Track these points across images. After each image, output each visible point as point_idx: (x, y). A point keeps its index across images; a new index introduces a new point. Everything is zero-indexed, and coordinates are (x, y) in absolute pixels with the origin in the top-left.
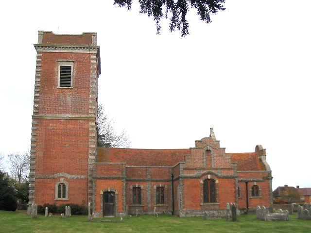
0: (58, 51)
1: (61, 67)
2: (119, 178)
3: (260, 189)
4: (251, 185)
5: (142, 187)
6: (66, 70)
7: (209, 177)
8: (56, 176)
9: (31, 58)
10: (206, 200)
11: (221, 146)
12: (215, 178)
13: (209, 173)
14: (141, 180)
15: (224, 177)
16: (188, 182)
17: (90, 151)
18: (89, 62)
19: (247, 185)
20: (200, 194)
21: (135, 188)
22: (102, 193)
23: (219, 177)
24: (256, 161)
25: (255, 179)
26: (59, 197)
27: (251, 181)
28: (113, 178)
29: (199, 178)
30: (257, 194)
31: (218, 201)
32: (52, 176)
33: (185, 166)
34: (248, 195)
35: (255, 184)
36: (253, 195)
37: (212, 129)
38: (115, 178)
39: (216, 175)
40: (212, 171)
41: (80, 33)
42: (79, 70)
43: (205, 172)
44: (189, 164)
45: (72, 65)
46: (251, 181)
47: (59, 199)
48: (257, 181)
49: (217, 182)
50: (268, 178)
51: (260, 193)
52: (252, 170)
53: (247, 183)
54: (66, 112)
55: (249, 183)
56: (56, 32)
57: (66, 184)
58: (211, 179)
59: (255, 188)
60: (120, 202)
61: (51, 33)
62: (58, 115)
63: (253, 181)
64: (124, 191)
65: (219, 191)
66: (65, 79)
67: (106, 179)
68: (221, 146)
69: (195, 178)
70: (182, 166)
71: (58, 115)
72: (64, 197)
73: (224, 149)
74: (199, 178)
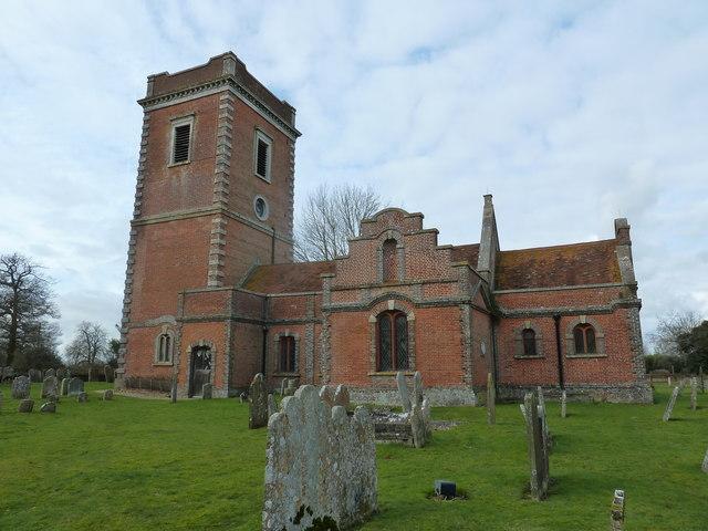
0: (171, 103)
1: (177, 129)
2: (219, 320)
3: (599, 334)
4: (570, 324)
7: (391, 305)
8: (156, 321)
9: (134, 121)
10: (382, 365)
11: (427, 225)
14: (295, 323)
15: (429, 305)
16: (341, 321)
17: (210, 273)
19: (557, 325)
20: (370, 346)
21: (283, 339)
22: (189, 350)
24: (602, 266)
26: (161, 359)
27: (572, 314)
29: (366, 309)
30: (592, 347)
31: (412, 365)
32: (151, 322)
33: (334, 283)
34: (563, 350)
35: (583, 319)
36: (579, 349)
37: (488, 198)
39: (409, 301)
40: (397, 290)
41: (206, 61)
43: (380, 293)
44: (344, 278)
45: (189, 122)
46: (572, 314)
47: (160, 363)
48: (588, 313)
49: (411, 316)
50: (630, 301)
51: (600, 345)
52: (586, 283)
54: (178, 206)
55: (565, 319)
56: (171, 72)
58: (395, 311)
60: (219, 372)
61: (164, 75)
62: (167, 214)
63: (577, 313)
64: (228, 345)
66: (181, 152)
68: (427, 225)
69: (357, 309)
70: (326, 284)
72: (167, 360)
73: (436, 232)
74: (366, 309)
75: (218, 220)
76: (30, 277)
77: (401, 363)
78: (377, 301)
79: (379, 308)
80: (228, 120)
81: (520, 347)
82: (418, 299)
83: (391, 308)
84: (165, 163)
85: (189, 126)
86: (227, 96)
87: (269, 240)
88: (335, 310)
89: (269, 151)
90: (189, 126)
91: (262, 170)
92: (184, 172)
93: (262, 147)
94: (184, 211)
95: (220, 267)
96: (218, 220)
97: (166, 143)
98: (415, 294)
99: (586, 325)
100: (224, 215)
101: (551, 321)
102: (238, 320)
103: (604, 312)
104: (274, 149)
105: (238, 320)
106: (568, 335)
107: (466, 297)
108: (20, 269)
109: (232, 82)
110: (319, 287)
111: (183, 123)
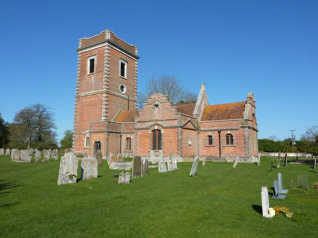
2: (103, 132)
4: (224, 134)
5: (131, 138)
6: (92, 61)
7: (156, 127)
8: (85, 132)
12: (160, 128)
13: (155, 125)
15: (168, 128)
16: (140, 133)
18: (104, 53)
21: (127, 138)
22: (94, 143)
23: (164, 128)
25: (229, 128)
28: (100, 132)
29: (148, 129)
30: (232, 143)
35: (229, 132)
38: (101, 132)
39: (162, 126)
42: (98, 59)
47: (86, 147)
48: (231, 130)
49: (162, 131)
53: (219, 132)
54: (91, 90)
55: (222, 133)
57: (232, 134)
59: (229, 136)
62: (87, 93)
65: (164, 140)
66: (92, 70)
67: (96, 133)
69: (145, 129)
71: (87, 93)
74: (148, 129)
75: (105, 95)
76: (45, 113)
77: (160, 148)
78: (152, 126)
79: (152, 129)
80: (108, 57)
81: (208, 142)
82: (165, 126)
83: (156, 129)
84: (86, 73)
85: (94, 59)
86: (107, 47)
87: (127, 101)
88: (139, 129)
89: (126, 66)
90: (94, 59)
91: (123, 74)
92: (93, 77)
93: (123, 65)
94: (93, 92)
95: (106, 112)
96: (105, 95)
97: (86, 65)
98: (165, 124)
99: (229, 134)
100: (107, 93)
101: (217, 132)
102: (110, 132)
103: (237, 130)
104: (127, 65)
105: (110, 132)
106: (224, 138)
107: (179, 125)
108: (41, 110)
109: (109, 42)
110: (133, 120)
111: (92, 58)
